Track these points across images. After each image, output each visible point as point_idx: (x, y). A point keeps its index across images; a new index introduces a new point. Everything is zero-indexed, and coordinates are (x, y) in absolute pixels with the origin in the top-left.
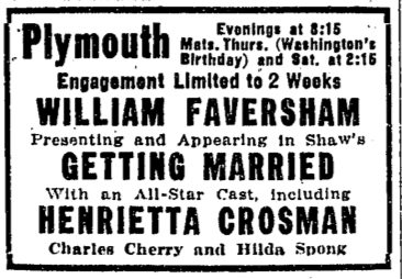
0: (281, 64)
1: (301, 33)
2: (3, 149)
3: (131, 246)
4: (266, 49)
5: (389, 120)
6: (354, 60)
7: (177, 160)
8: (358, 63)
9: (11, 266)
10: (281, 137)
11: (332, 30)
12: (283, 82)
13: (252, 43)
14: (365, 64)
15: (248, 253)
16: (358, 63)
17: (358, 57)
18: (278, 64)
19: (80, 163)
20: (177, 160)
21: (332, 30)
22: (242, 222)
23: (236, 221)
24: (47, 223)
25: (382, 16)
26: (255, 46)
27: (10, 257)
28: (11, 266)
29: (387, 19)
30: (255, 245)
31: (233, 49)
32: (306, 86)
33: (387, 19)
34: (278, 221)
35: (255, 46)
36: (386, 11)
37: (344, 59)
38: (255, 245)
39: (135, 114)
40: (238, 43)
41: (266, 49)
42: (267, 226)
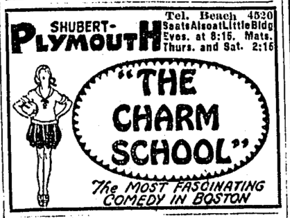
0: (217, 50)
1: (204, 39)
2: (274, 78)
4: (188, 39)
5: (10, 155)
6: (258, 48)
8: (260, 50)
11: (268, 47)
12: (166, 41)
13: (184, 46)
14: (266, 50)
15: (74, 23)
16: (260, 50)
17: (260, 46)
18: (215, 50)
19: (84, 25)
21: (268, 47)
25: (14, 208)
26: (186, 48)
31: (170, 50)
35: (186, 48)
37: (221, 46)
40: (173, 46)
41: (188, 39)
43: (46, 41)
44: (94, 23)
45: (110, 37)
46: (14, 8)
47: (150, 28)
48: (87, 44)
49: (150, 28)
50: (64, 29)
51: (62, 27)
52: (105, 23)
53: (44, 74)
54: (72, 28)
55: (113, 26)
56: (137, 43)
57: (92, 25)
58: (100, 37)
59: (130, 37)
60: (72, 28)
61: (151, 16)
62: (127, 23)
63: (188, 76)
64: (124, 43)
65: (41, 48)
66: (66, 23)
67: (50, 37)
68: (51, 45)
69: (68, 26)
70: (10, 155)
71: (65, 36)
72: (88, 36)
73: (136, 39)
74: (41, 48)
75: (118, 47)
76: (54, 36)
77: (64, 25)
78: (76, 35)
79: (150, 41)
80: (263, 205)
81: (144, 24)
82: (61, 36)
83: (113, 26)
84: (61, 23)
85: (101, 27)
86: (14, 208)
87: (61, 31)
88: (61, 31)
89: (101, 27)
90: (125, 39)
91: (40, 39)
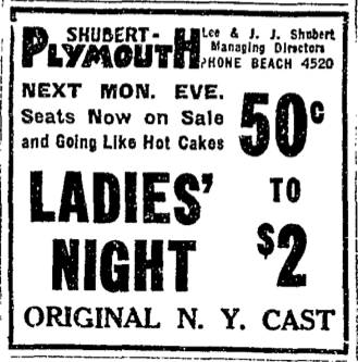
3: (272, 316)
5: (11, 226)
7: (115, 255)
9: (12, 347)
10: (166, 122)
15: (99, 29)
20: (115, 255)
22: (286, 63)
23: (283, 63)
24: (149, 272)
27: (11, 338)
28: (12, 347)
29: (339, 352)
30: (210, 123)
32: (224, 50)
33: (339, 352)
34: (217, 145)
36: (345, 15)
38: (210, 123)
39: (81, 198)
42: (293, 185)
43: (61, 54)
44: (128, 29)
45: (138, 49)
46: (342, 290)
47: (188, 37)
48: (305, 110)
49: (188, 37)
50: (84, 38)
51: (81, 34)
52: (144, 30)
53: (61, 139)
54: (96, 37)
55: (156, 36)
56: (171, 57)
57: (124, 32)
58: (126, 49)
59: (164, 50)
60: (96, 37)
61: (189, 23)
62: (163, 30)
63: (211, 89)
64: (156, 56)
65: (54, 61)
66: (87, 29)
67: (64, 46)
68: (66, 58)
69: (90, 34)
70: (11, 226)
71: (84, 46)
72: (113, 47)
73: (171, 51)
74: (54, 61)
75: (148, 63)
76: (71, 47)
77: (84, 31)
78: (99, 45)
79: (187, 55)
80: (342, 271)
81: (179, 32)
82: (78, 46)
83: (156, 36)
84: (81, 29)
85: (139, 35)
86: (16, 342)
87: (81, 40)
88: (81, 40)
89: (139, 35)
90: (156, 51)
91: (53, 47)
